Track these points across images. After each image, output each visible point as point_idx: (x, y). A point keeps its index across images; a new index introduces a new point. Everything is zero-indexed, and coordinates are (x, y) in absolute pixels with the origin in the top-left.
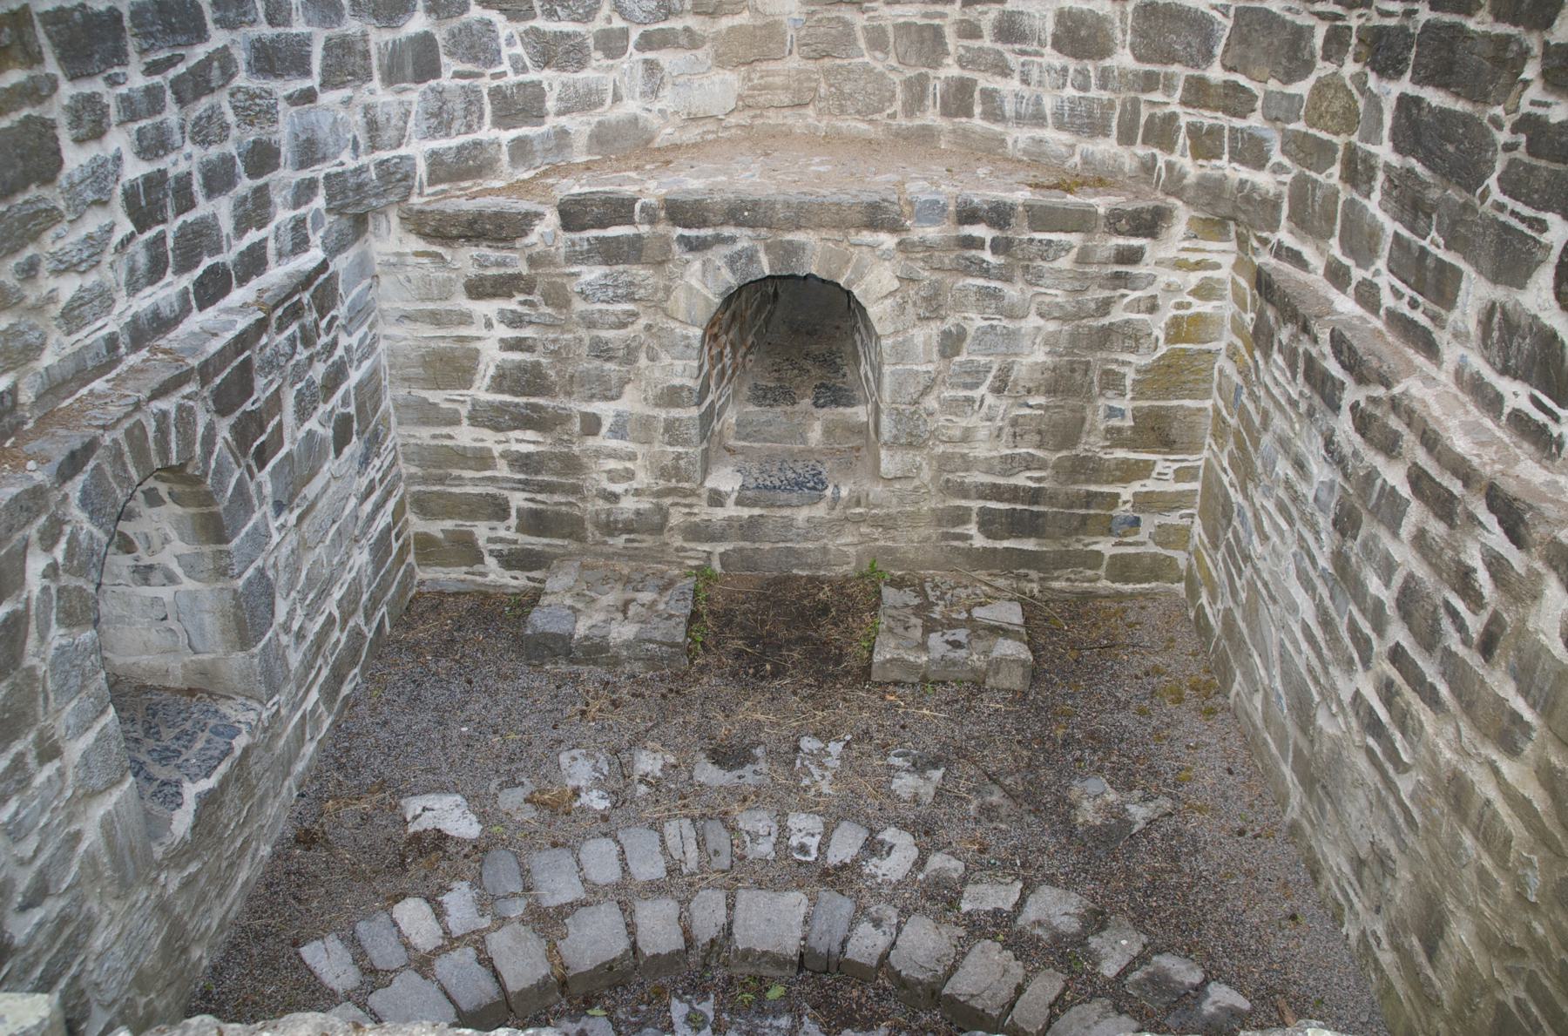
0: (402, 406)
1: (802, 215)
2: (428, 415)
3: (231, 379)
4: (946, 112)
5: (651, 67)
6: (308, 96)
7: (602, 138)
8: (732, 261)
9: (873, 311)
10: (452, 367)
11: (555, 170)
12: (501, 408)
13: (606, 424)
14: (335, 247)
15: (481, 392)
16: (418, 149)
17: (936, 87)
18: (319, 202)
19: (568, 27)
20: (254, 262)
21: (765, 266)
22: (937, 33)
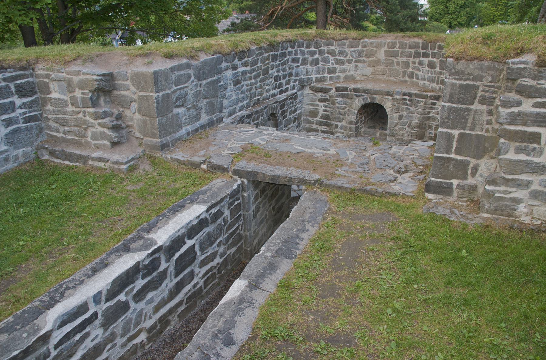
0: (305, 120)
1: (376, 92)
2: (309, 122)
3: (282, 103)
4: (409, 78)
5: (356, 66)
6: (298, 66)
7: (346, 78)
8: (363, 99)
9: (387, 110)
10: (314, 114)
11: (337, 82)
12: (321, 122)
13: (339, 127)
14: (298, 91)
15: (318, 118)
16: (314, 76)
17: (408, 73)
18: (297, 83)
19: (342, 58)
20: (287, 90)
21: (369, 101)
22: (408, 63)
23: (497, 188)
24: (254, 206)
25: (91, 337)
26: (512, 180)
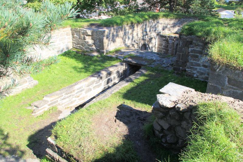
23: (189, 70)
25: (93, 87)
26: (192, 67)
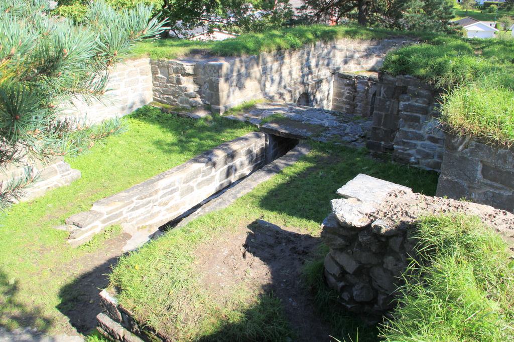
23: (399, 147)
24: (273, 151)
